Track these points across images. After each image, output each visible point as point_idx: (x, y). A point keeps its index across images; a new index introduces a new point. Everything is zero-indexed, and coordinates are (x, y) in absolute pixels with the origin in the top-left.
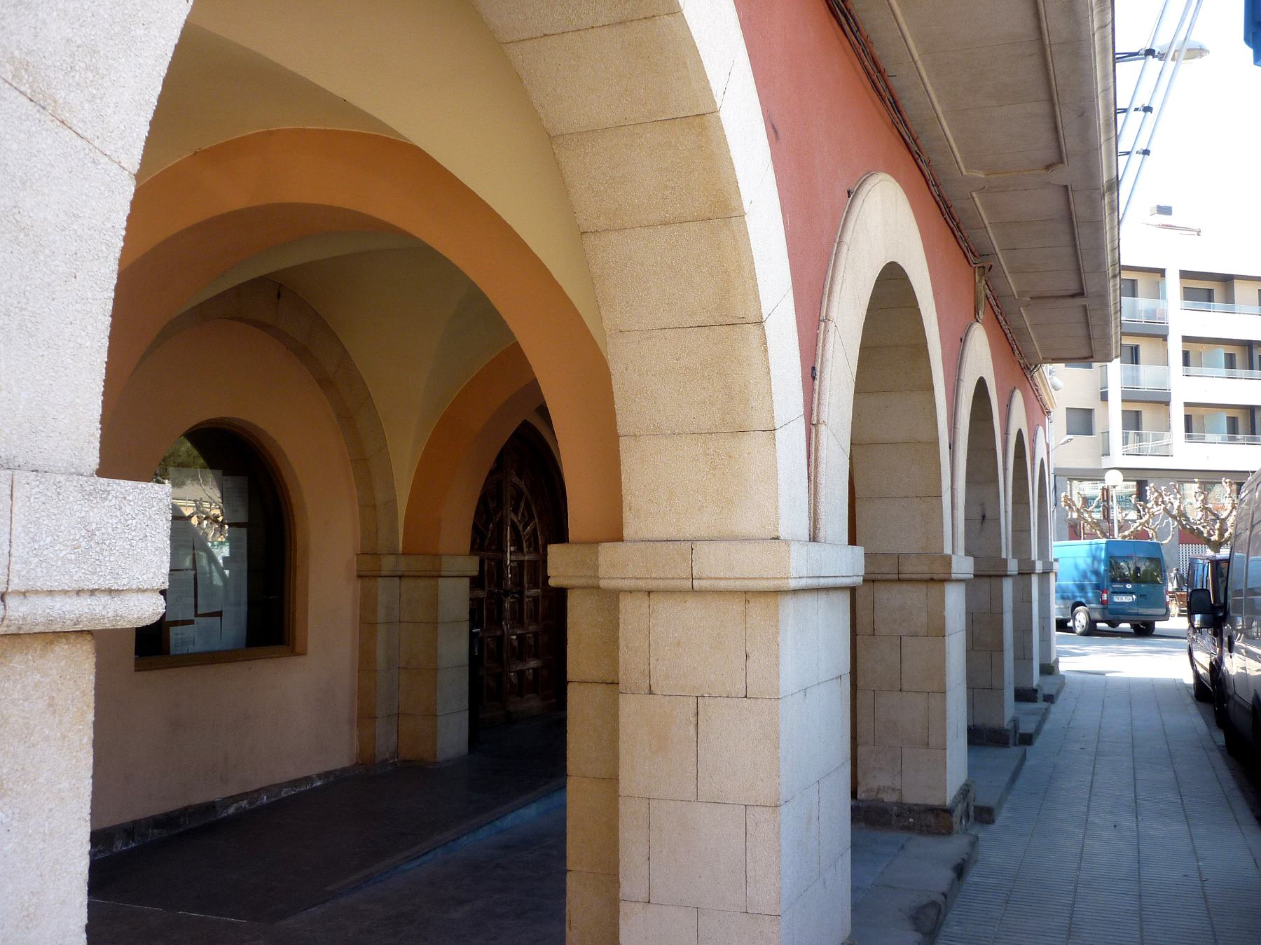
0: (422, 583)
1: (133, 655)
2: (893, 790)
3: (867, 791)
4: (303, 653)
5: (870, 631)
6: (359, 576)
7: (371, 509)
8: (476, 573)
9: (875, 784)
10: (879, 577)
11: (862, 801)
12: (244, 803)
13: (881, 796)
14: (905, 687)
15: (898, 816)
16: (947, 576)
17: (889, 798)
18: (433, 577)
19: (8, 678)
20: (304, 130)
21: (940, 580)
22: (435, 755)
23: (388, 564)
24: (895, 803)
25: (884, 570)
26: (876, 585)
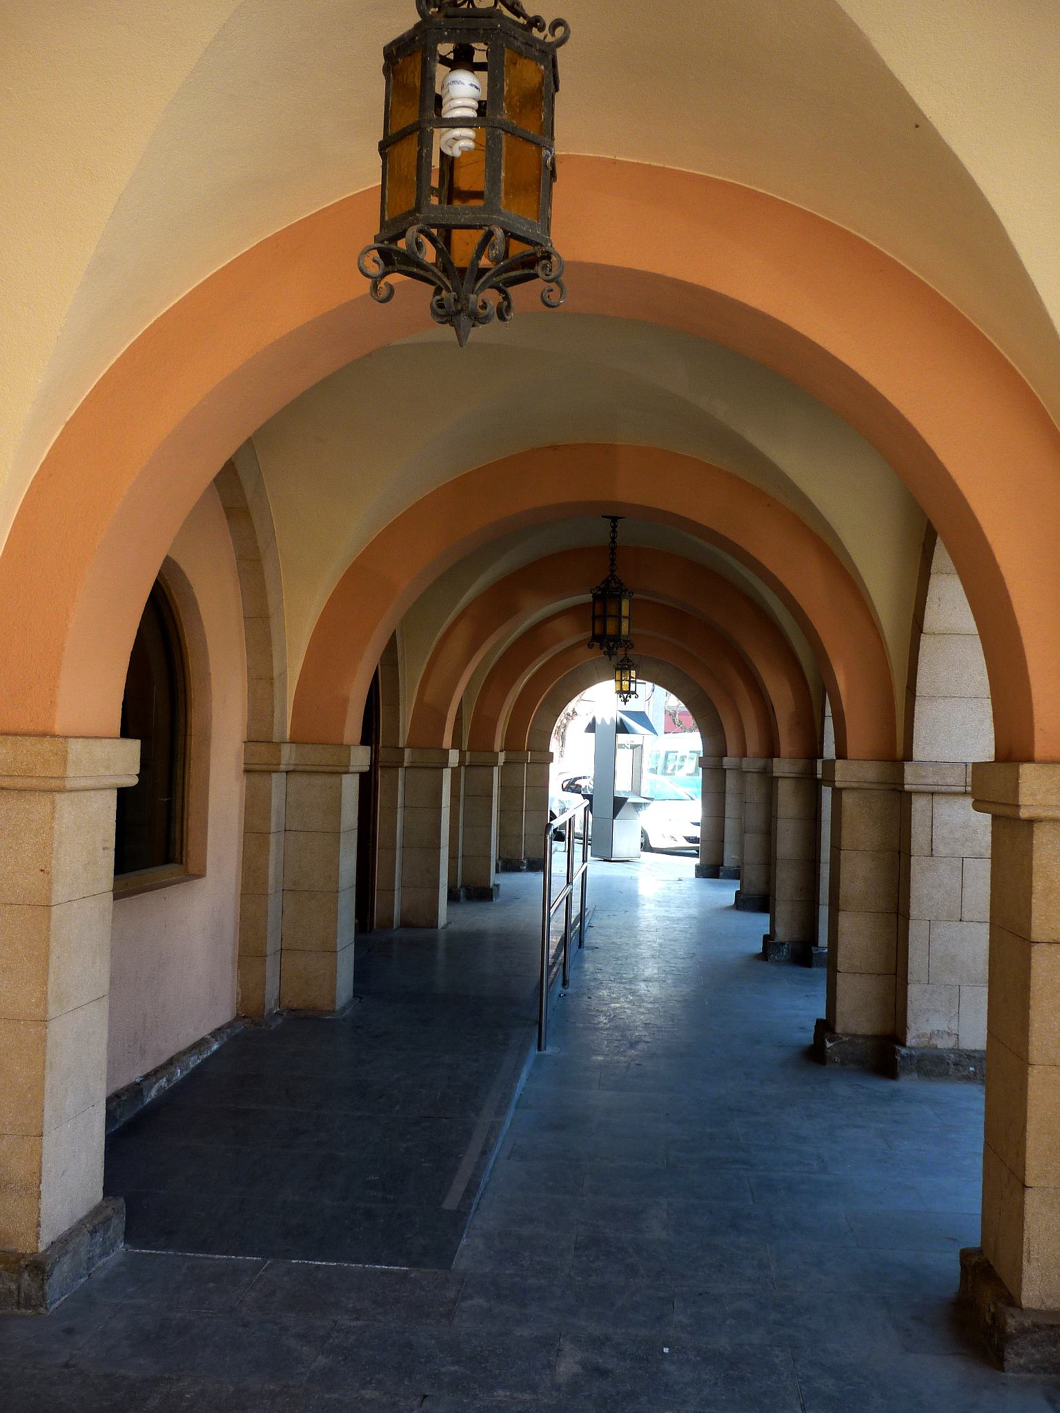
0: (319, 780)
1: (112, 875)
2: (949, 1034)
3: (918, 1036)
4: (201, 875)
5: (928, 852)
6: (247, 771)
7: (262, 680)
8: (367, 769)
9: (928, 1029)
10: (943, 789)
11: (911, 1048)
12: (163, 1082)
13: (934, 1042)
14: (966, 916)
15: (956, 1064)
16: (275, 768)
17: (943, 1043)
18: (333, 773)
19: (661, 945)
20: (615, 162)
21: (339, 771)
22: (333, 1002)
23: (288, 755)
24: (951, 1050)
25: (950, 781)
26: (936, 798)
